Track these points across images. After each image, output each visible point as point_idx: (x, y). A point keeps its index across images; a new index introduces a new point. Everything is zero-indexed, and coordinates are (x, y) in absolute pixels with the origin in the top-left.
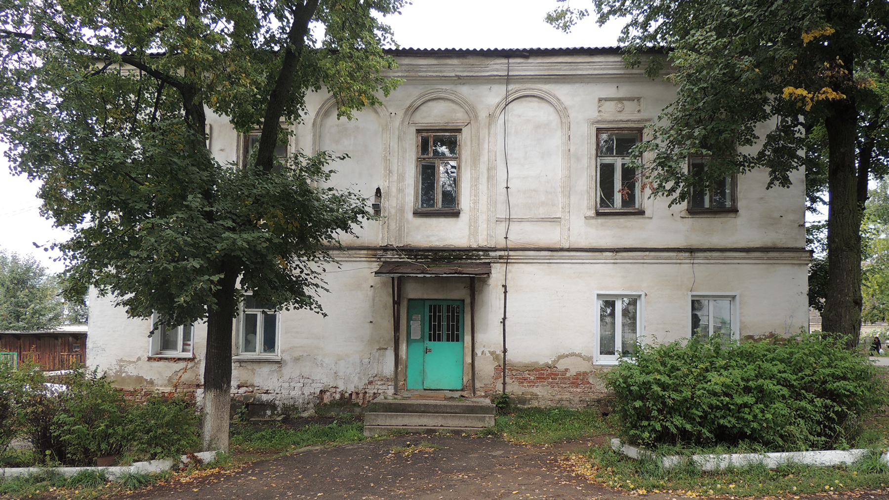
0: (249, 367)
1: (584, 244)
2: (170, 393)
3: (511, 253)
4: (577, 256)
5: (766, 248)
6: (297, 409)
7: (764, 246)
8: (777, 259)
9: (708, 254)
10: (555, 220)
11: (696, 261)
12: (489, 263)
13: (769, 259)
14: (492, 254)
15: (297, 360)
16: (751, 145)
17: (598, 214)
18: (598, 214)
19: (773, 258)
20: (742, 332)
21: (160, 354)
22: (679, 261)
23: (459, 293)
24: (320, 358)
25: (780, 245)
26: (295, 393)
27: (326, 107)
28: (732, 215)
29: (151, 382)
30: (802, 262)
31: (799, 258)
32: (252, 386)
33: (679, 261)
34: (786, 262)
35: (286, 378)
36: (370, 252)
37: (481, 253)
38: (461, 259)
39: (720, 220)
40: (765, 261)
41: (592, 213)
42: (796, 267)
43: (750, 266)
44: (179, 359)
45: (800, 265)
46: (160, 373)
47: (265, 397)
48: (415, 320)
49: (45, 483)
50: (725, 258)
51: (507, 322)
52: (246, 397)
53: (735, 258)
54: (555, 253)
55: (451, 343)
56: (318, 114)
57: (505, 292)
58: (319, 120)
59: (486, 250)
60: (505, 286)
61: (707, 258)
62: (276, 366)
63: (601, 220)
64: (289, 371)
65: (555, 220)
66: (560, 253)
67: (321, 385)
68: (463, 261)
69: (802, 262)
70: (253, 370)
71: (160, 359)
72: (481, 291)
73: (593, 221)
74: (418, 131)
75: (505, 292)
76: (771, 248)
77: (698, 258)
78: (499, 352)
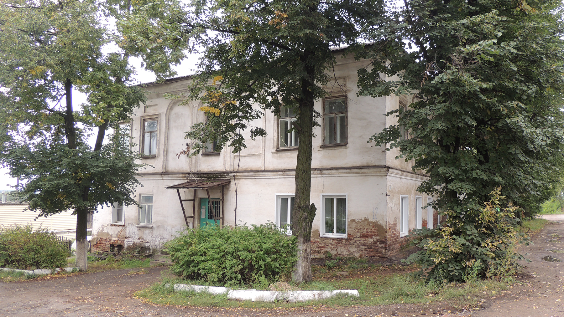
0: (142, 230)
1: (271, 167)
2: (117, 241)
3: (238, 174)
4: (260, 175)
5: (363, 166)
6: (157, 251)
7: (362, 165)
8: (367, 173)
9: (329, 171)
10: (259, 155)
11: (324, 176)
12: (229, 179)
13: (363, 173)
14: (230, 174)
15: (158, 227)
16: (180, 63)
17: (278, 151)
18: (278, 151)
19: (365, 173)
20: (349, 217)
21: (117, 223)
22: (315, 176)
23: (218, 195)
24: (166, 226)
25: (371, 164)
26: (157, 243)
27: (171, 106)
28: (344, 147)
29: (111, 236)
30: (383, 174)
31: (380, 172)
32: (143, 239)
33: (315, 176)
34: (373, 174)
35: (154, 236)
36: (183, 175)
37: (225, 174)
38: (218, 177)
39: (338, 150)
40: (361, 175)
41: (274, 150)
42: (380, 178)
43: (353, 177)
44: (120, 225)
45: (381, 176)
46: (114, 232)
47: (147, 245)
48: (203, 208)
49: (427, 256)
50: (339, 173)
51: (237, 210)
52: (141, 244)
53: (344, 173)
54: (256, 174)
55: (211, 220)
56: (167, 110)
57: (236, 194)
58: (168, 112)
59: (227, 173)
60: (236, 191)
61: (329, 174)
62: (150, 230)
63: (279, 154)
64: (156, 233)
65: (259, 155)
66: (258, 173)
67: (166, 240)
68: (219, 179)
69: (383, 174)
70: (143, 231)
71: (115, 225)
72: (227, 194)
73: (276, 155)
74: (205, 113)
75: (236, 194)
76: (366, 166)
77: (324, 174)
78: (233, 226)
